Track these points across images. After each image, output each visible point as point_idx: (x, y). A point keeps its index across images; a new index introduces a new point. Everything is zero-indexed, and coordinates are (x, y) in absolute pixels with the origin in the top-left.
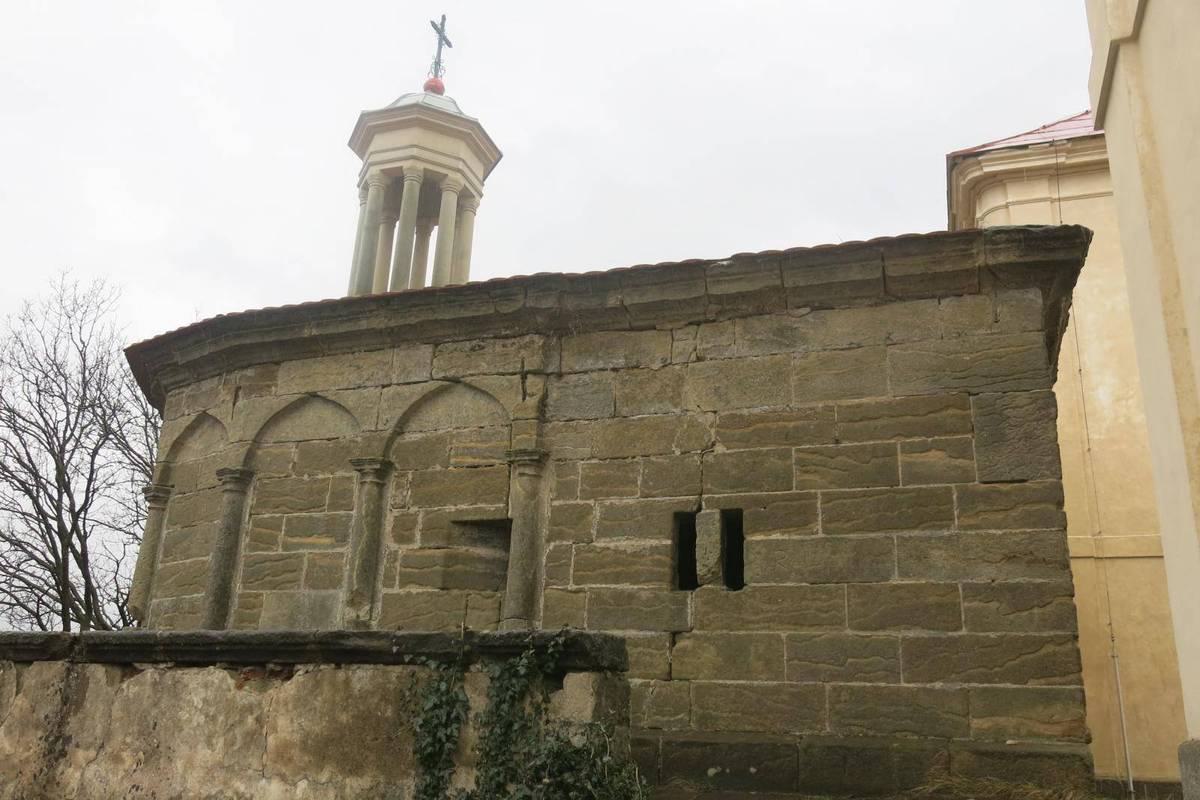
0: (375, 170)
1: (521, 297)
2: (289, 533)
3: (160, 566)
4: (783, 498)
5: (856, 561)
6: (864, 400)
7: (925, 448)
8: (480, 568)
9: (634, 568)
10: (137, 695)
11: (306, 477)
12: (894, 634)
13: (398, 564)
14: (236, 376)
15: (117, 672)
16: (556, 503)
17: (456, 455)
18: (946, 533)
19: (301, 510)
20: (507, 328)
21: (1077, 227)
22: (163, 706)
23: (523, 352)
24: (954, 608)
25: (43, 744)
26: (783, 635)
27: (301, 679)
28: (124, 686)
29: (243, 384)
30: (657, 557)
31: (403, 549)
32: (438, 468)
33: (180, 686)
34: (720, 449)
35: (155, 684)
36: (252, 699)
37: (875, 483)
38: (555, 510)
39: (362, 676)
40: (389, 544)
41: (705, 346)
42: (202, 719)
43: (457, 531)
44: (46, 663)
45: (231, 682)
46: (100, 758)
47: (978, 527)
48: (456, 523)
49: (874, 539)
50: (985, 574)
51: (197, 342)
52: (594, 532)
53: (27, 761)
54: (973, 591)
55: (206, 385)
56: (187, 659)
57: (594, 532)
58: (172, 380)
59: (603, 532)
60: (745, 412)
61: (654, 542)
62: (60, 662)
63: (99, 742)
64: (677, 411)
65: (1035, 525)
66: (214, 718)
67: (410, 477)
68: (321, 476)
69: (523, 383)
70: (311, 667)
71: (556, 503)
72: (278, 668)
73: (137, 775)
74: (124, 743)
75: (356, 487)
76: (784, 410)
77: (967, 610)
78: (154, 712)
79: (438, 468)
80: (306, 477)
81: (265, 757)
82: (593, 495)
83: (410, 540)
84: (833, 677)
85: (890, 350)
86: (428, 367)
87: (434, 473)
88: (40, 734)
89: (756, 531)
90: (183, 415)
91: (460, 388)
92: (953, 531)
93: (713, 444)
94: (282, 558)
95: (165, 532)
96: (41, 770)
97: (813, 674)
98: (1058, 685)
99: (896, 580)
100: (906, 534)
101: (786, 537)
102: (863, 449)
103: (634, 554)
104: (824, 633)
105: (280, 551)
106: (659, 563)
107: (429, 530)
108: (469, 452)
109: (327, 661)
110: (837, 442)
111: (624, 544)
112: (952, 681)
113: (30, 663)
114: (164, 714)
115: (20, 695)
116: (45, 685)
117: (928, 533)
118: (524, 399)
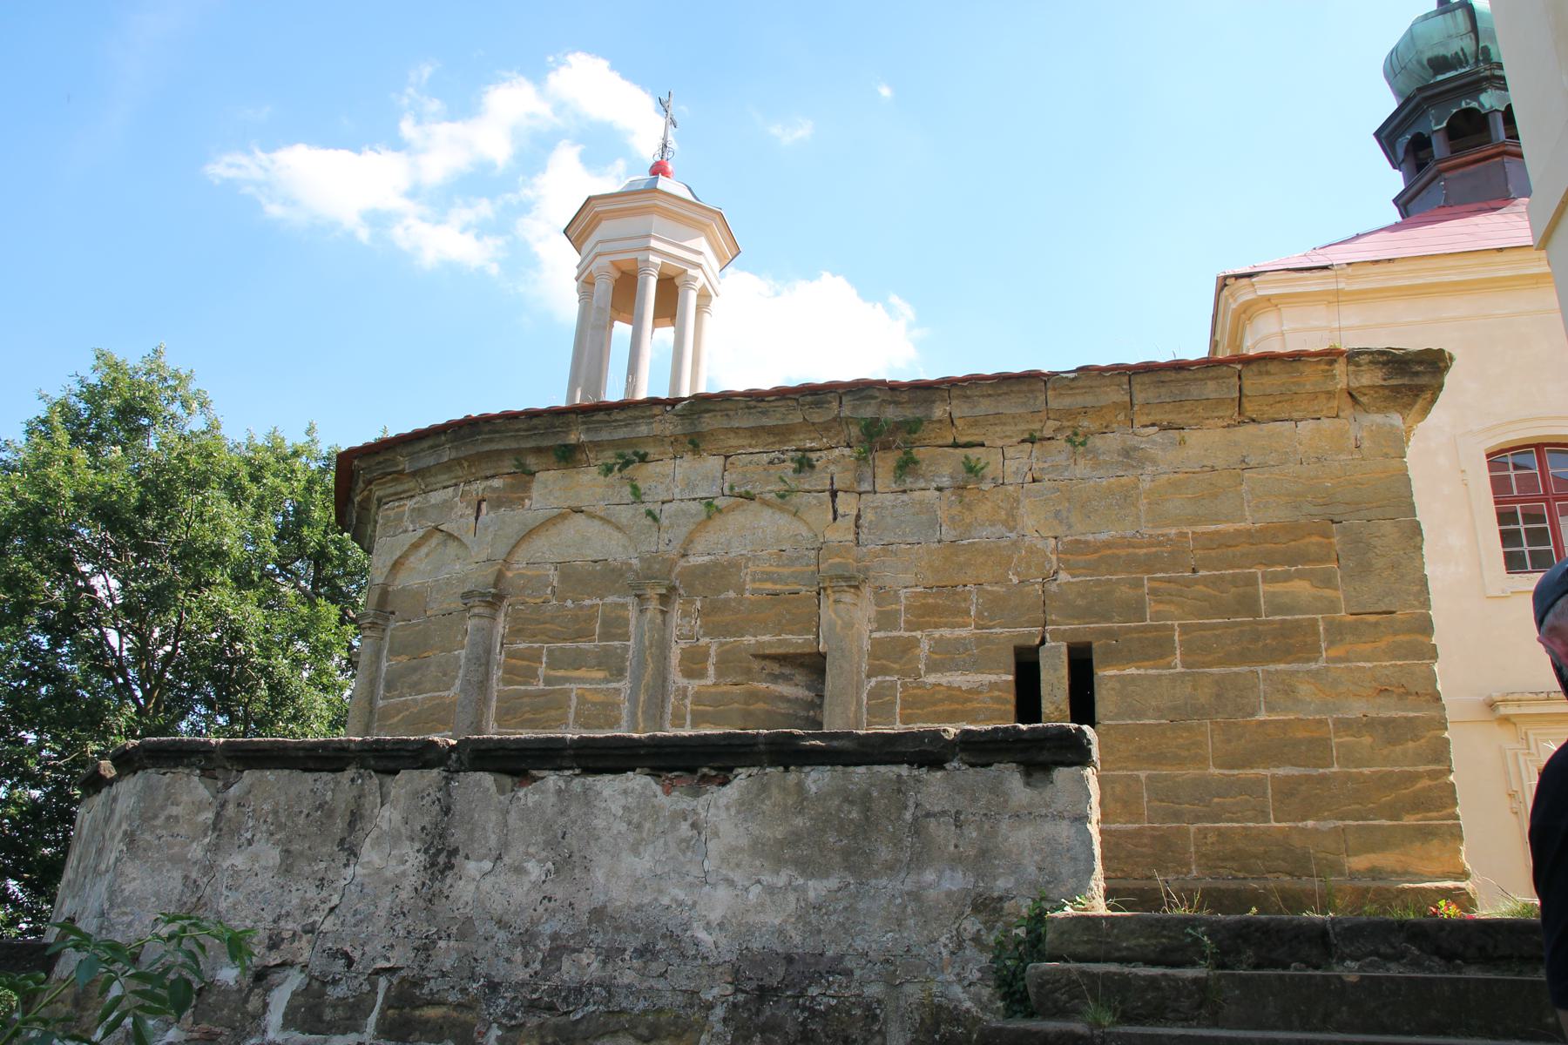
0: (604, 261)
1: (835, 404)
2: (550, 666)
3: (381, 703)
4: (1136, 629)
5: (1218, 696)
6: (1220, 527)
7: (1288, 577)
8: (783, 708)
9: (969, 706)
10: (538, 805)
11: (569, 603)
12: (1263, 772)
13: (688, 702)
14: (479, 487)
15: (507, 781)
16: (875, 635)
17: (753, 581)
18: (1313, 666)
19: (565, 640)
20: (812, 440)
21: (1441, 351)
22: (572, 814)
23: (832, 468)
24: (1324, 743)
25: (422, 857)
26: (1143, 775)
27: (744, 783)
28: (521, 794)
29: (487, 495)
30: (997, 693)
31: (694, 685)
32: (732, 594)
33: (591, 793)
34: (1063, 577)
35: (559, 791)
36: (684, 806)
37: (1237, 613)
38: (876, 643)
39: (817, 779)
40: (677, 678)
41: (1041, 465)
42: (623, 827)
43: (756, 665)
44: (417, 772)
45: (658, 789)
46: (498, 869)
47: (1347, 660)
48: (755, 656)
49: (1237, 674)
50: (1357, 709)
51: (431, 447)
52: (922, 666)
53: (404, 874)
54: (1345, 725)
55: (436, 497)
56: (600, 765)
57: (922, 666)
58: (392, 490)
59: (933, 667)
60: (1090, 537)
61: (993, 678)
62: (435, 771)
63: (495, 853)
64: (1013, 535)
65: (1406, 658)
66: (639, 826)
67: (698, 605)
68: (587, 602)
69: (833, 502)
70: (754, 770)
71: (875, 635)
72: (713, 773)
73: (548, 887)
74: (527, 854)
75: (632, 614)
76: (1134, 536)
77: (1339, 745)
78: (562, 820)
79: (732, 594)
80: (569, 603)
81: (706, 863)
82: (920, 627)
83: (701, 674)
84: (1198, 819)
85: (1247, 474)
86: (719, 481)
87: (727, 601)
88: (417, 846)
89: (1107, 664)
90: (406, 531)
91: (754, 505)
92: (1321, 664)
93: (1056, 572)
94: (543, 694)
95: (385, 665)
96: (424, 884)
97: (1177, 816)
98: (1434, 820)
99: (1262, 716)
100: (1272, 667)
101: (1142, 672)
102: (1222, 578)
103: (969, 691)
104: (1191, 772)
105: (541, 686)
106: (997, 700)
107: (726, 664)
108: (769, 577)
109: (773, 764)
110: (1194, 571)
111: (959, 680)
112: (1324, 819)
113: (397, 772)
114: (574, 822)
115: (387, 806)
116: (417, 795)
117: (1295, 666)
118: (835, 519)
